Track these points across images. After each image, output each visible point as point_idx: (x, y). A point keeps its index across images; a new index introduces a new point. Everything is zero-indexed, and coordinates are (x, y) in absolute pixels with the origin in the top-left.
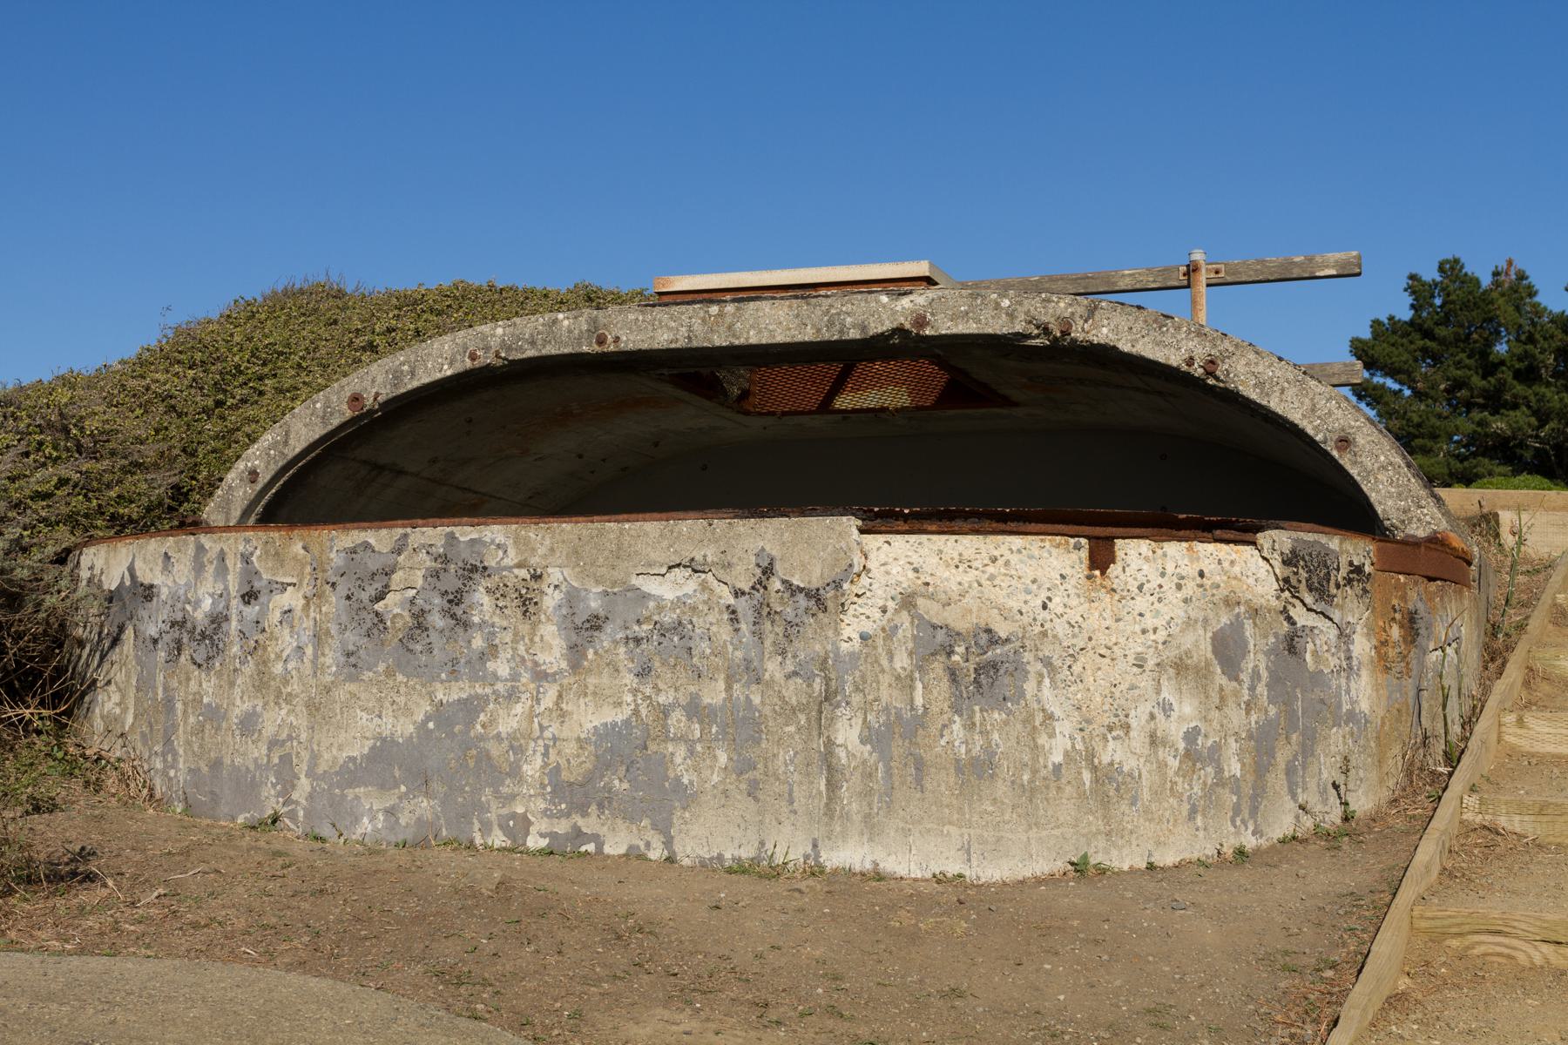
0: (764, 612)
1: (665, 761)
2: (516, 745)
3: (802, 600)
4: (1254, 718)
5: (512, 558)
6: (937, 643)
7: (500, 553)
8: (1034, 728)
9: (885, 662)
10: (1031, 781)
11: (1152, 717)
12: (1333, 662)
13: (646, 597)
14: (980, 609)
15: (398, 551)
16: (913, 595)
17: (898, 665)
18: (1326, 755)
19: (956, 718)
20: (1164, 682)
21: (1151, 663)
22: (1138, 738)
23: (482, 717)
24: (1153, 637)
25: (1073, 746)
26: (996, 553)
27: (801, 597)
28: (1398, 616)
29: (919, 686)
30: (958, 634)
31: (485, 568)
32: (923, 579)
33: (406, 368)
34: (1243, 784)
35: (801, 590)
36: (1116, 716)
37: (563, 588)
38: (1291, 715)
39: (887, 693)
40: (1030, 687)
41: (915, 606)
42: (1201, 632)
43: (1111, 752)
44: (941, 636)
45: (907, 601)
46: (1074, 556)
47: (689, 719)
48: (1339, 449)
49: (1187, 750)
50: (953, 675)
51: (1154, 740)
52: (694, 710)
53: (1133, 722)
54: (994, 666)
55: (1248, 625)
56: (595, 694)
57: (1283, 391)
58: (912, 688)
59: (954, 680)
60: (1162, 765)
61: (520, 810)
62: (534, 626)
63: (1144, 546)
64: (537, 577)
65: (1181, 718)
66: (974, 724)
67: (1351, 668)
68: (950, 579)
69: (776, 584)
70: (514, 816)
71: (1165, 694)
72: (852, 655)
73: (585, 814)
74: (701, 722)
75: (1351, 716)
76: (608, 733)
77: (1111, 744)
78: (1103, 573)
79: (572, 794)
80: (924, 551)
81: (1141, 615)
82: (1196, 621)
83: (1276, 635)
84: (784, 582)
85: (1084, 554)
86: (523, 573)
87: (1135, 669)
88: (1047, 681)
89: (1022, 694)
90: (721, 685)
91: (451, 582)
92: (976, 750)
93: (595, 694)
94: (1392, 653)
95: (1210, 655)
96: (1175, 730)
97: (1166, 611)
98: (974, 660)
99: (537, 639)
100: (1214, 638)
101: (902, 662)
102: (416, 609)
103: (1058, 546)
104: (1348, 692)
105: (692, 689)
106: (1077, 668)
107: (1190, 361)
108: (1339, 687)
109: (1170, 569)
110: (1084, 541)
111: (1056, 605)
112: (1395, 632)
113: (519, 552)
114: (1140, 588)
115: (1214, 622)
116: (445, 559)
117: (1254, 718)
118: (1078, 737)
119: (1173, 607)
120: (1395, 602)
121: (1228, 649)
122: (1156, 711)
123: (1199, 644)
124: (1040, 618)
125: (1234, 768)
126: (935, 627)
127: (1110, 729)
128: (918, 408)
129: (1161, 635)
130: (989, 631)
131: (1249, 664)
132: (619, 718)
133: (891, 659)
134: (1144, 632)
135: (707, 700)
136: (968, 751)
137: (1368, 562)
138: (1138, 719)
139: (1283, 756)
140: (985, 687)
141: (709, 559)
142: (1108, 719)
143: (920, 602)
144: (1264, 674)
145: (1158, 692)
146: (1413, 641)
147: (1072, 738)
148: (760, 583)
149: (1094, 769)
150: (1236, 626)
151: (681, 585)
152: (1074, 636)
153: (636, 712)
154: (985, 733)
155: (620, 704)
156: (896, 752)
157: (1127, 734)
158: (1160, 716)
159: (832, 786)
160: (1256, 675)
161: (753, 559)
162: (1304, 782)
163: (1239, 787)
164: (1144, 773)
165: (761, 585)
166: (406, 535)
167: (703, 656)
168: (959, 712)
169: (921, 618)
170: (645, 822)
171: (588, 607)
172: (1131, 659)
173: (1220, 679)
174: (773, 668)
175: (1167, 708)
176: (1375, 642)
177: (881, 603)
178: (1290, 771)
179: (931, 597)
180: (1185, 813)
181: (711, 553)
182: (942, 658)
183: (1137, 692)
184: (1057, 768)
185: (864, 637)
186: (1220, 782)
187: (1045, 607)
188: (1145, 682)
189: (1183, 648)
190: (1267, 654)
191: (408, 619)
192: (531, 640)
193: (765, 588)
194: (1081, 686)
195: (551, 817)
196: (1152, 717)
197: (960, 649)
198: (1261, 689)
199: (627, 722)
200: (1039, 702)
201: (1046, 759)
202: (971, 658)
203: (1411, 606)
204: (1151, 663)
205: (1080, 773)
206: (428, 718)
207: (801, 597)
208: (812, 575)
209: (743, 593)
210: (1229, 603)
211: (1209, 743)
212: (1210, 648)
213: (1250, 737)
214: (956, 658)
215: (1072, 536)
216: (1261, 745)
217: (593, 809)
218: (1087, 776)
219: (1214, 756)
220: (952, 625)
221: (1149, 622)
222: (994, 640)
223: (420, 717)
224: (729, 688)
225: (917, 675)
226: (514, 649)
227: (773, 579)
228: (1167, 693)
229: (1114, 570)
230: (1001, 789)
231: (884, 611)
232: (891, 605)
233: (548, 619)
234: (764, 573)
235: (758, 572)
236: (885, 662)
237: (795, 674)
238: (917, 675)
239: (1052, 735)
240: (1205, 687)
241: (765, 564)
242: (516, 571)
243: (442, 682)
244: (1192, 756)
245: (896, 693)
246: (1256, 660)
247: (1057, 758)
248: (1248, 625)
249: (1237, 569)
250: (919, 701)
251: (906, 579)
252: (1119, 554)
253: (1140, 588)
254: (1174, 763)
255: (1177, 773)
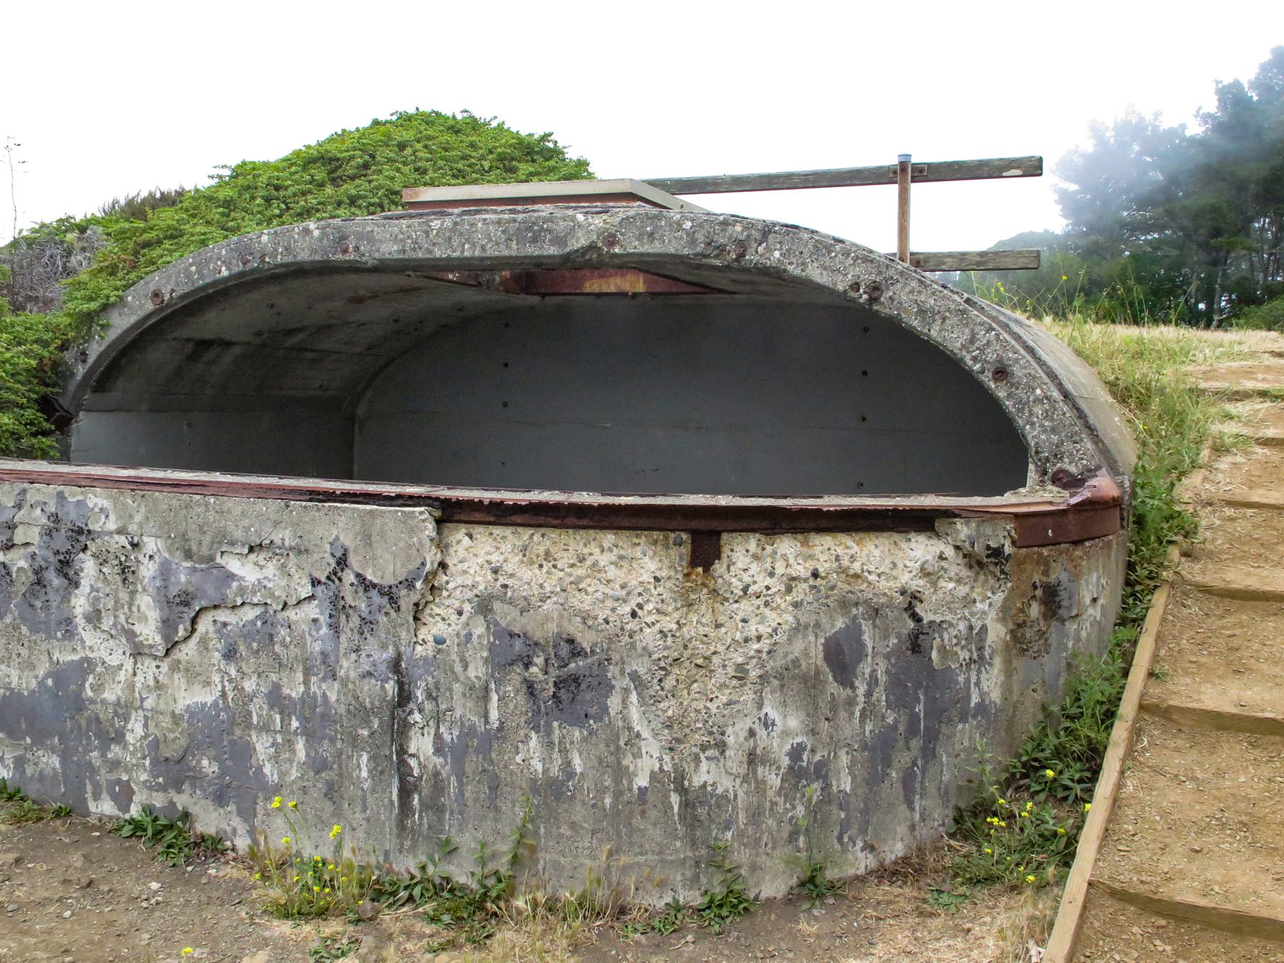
0: (338, 607)
1: (250, 749)
2: (123, 709)
3: (377, 599)
4: (869, 727)
5: (112, 525)
6: (511, 651)
7: (103, 517)
8: (618, 748)
9: (458, 668)
10: (613, 806)
11: (752, 733)
12: (964, 655)
13: (231, 576)
14: (561, 616)
15: (19, 506)
16: (491, 597)
17: (472, 673)
18: (949, 756)
19: (533, 735)
20: (768, 697)
21: (754, 674)
22: (735, 758)
23: (91, 679)
24: (756, 646)
25: (661, 768)
26: (586, 551)
27: (374, 593)
28: (1039, 592)
29: (495, 697)
30: (536, 644)
31: (89, 531)
32: (502, 580)
33: (193, 269)
34: (853, 799)
35: (374, 586)
36: (711, 733)
37: (156, 557)
38: (914, 719)
39: (463, 709)
40: (614, 703)
41: (491, 611)
42: (812, 638)
43: (704, 775)
44: (518, 645)
45: (484, 606)
46: (674, 552)
47: (271, 707)
48: (996, 380)
49: (791, 768)
50: (530, 688)
51: (753, 759)
52: (276, 698)
53: (731, 740)
54: (576, 680)
55: (866, 627)
56: (187, 670)
57: (944, 319)
58: (486, 698)
59: (532, 694)
60: (761, 786)
61: (125, 778)
62: (133, 594)
63: (752, 542)
64: (135, 546)
65: (786, 733)
66: (552, 743)
67: (981, 657)
68: (528, 579)
69: (349, 577)
70: (119, 781)
71: (767, 709)
72: (425, 659)
73: (179, 791)
74: (281, 713)
75: (982, 708)
76: (195, 713)
77: (704, 765)
78: (707, 570)
79: (174, 770)
80: (506, 547)
81: (744, 621)
82: (806, 627)
83: (899, 636)
84: (358, 575)
85: (686, 550)
86: (123, 540)
87: (735, 682)
88: (634, 697)
89: (605, 710)
90: (300, 676)
91: (61, 542)
92: (555, 771)
93: (187, 670)
94: (1029, 633)
95: (820, 661)
96: (781, 750)
97: (772, 617)
98: (554, 672)
99: (134, 609)
100: (827, 646)
101: (477, 671)
102: (36, 566)
103: (655, 543)
104: (978, 684)
105: (274, 677)
106: (670, 682)
107: (855, 287)
108: (968, 680)
109: (780, 569)
110: (684, 536)
111: (647, 616)
112: (1035, 610)
113: (119, 517)
114: (745, 590)
115: (827, 627)
116: (55, 518)
117: (869, 727)
118: (667, 758)
119: (781, 617)
120: (1036, 578)
121: (842, 658)
122: (756, 727)
123: (813, 651)
124: (628, 627)
125: (845, 783)
126: (511, 635)
127: (704, 748)
128: (653, 295)
129: (765, 645)
130: (571, 641)
131: (865, 668)
132: (209, 699)
133: (466, 667)
134: (746, 640)
135: (286, 691)
136: (545, 771)
137: (1007, 544)
138: (736, 735)
139: (902, 759)
140: (565, 705)
141: (287, 544)
142: (700, 738)
143: (497, 606)
144: (882, 678)
145: (760, 707)
146: (1054, 614)
147: (661, 759)
148: (335, 574)
149: (682, 791)
150: (853, 631)
151: (261, 567)
152: (666, 648)
153: (224, 694)
154: (564, 751)
155: (209, 684)
156: (469, 768)
157: (723, 752)
158: (761, 732)
159: (406, 793)
160: (873, 682)
161: (328, 547)
162: (923, 788)
163: (848, 803)
164: (741, 794)
165: (334, 576)
166: (24, 491)
167: (283, 644)
168: (536, 729)
169: (497, 624)
170: (231, 808)
171: (179, 582)
172: (731, 671)
173: (833, 687)
174: (346, 666)
175: (767, 724)
176: (1011, 626)
177: (457, 604)
178: (908, 781)
179: (511, 602)
180: (785, 835)
181: (284, 536)
182: (518, 669)
183: (737, 707)
184: (643, 791)
185: (439, 641)
186: (828, 796)
187: (634, 614)
188: (748, 696)
189: (791, 657)
190: (887, 657)
191: (30, 574)
192: (130, 609)
193: (340, 579)
194: (673, 702)
195: (151, 788)
196: (752, 733)
197: (539, 660)
198: (880, 694)
199: (215, 704)
200: (624, 719)
201: (630, 782)
202: (551, 670)
203: (1052, 578)
204: (754, 674)
205: (668, 797)
206: (47, 676)
207: (374, 593)
208: (385, 570)
209: (319, 582)
210: (844, 604)
211: (817, 758)
212: (821, 655)
213: (864, 747)
214: (534, 670)
215: (673, 531)
216: (879, 752)
217: (186, 787)
218: (675, 799)
219: (821, 772)
220: (530, 634)
221: (752, 629)
222: (576, 651)
223: (41, 673)
224: (306, 682)
225: (493, 686)
226: (116, 617)
227: (347, 571)
228: (771, 711)
229: (719, 568)
230: (579, 813)
231: (460, 613)
232: (467, 608)
233: (144, 590)
234: (338, 563)
235: (333, 562)
236: (458, 668)
237: (370, 674)
238: (493, 686)
239: (637, 755)
240: (814, 698)
241: (339, 554)
242: (116, 537)
243: (58, 640)
244: (796, 775)
245: (470, 704)
246: (874, 664)
247: (642, 781)
248: (866, 627)
249: (856, 567)
250: (494, 715)
251: (483, 581)
252: (726, 551)
253: (745, 590)
254: (774, 780)
255: (779, 793)
